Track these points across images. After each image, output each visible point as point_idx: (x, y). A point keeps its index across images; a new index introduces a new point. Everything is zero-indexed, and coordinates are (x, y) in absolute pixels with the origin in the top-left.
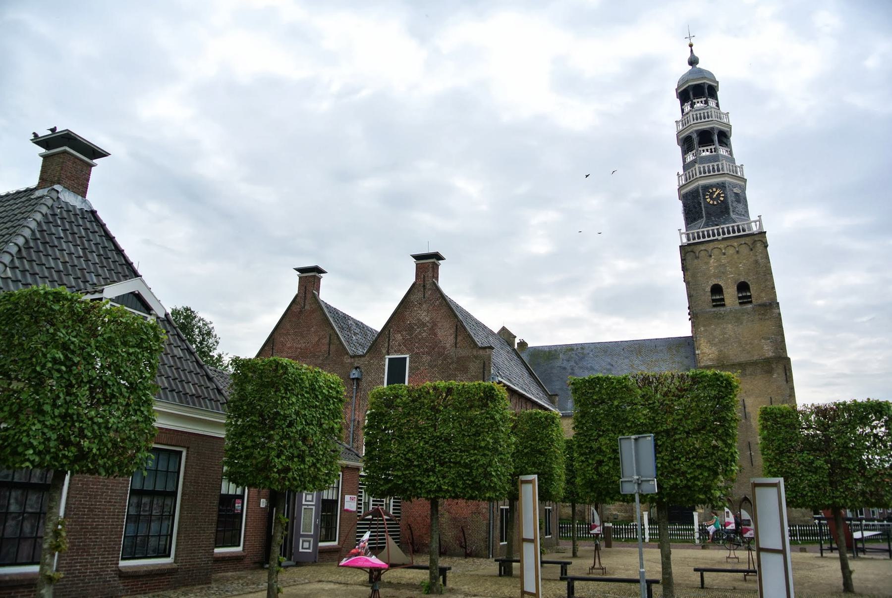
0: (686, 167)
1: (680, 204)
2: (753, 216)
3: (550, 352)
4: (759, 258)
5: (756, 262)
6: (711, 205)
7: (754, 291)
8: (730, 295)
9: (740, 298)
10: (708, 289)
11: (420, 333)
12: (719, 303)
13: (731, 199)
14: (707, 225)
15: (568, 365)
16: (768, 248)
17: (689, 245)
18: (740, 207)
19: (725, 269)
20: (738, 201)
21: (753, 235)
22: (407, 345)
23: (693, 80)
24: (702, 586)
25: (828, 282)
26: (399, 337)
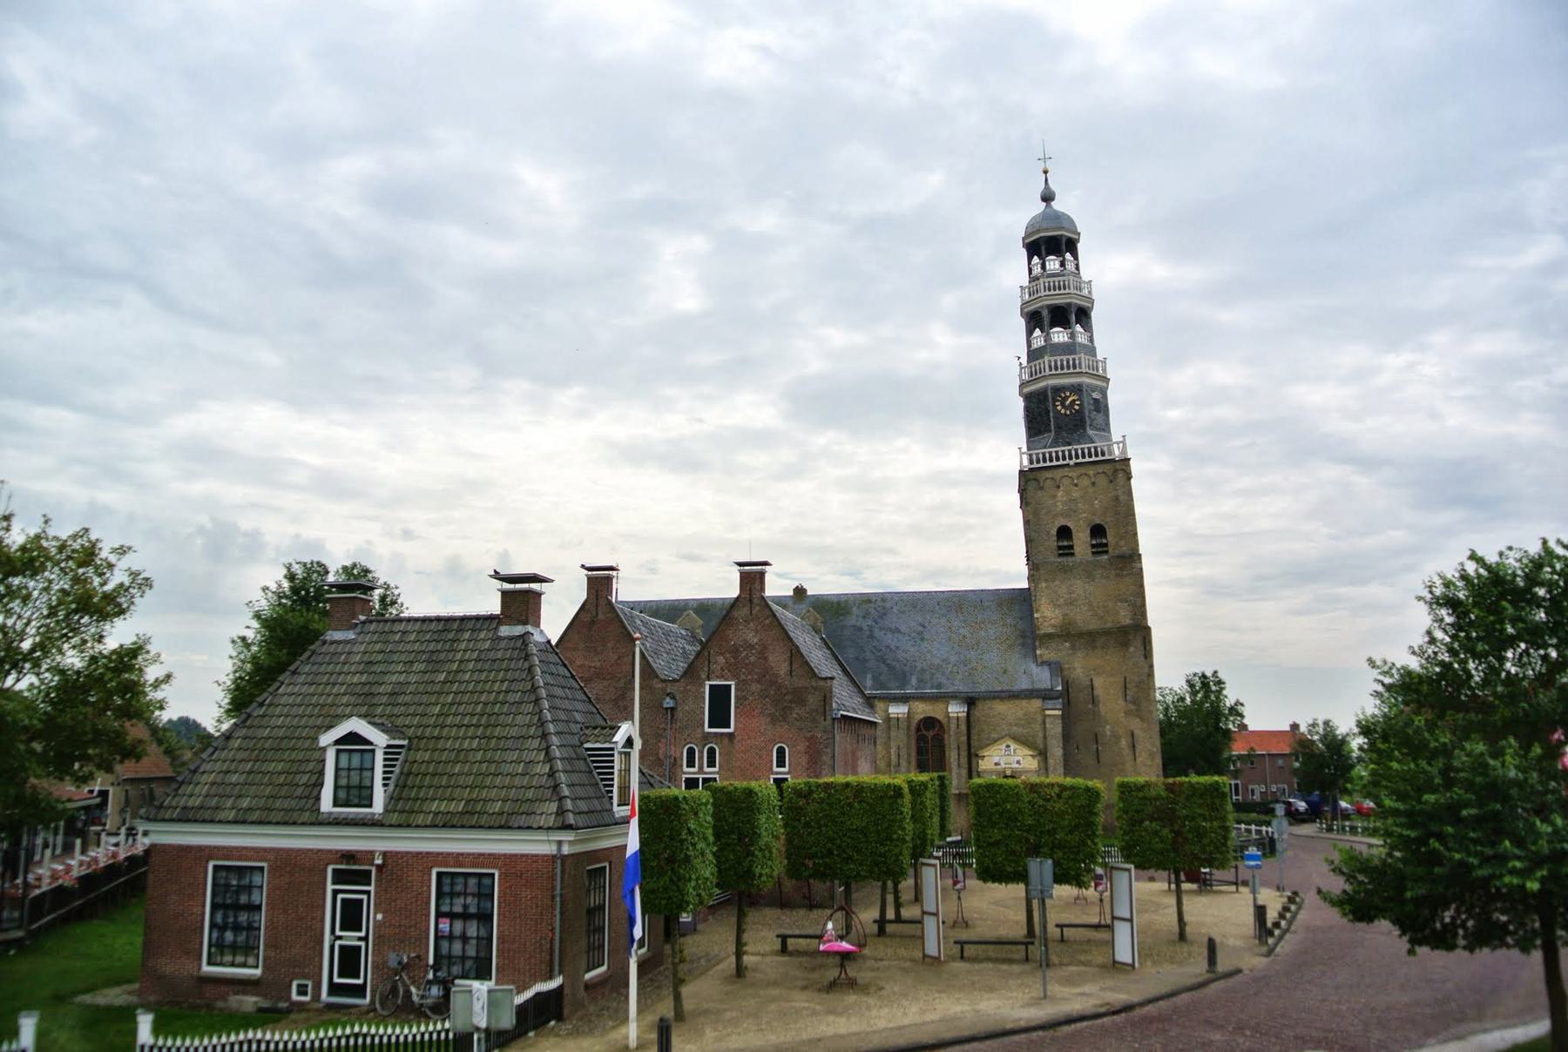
0: (1033, 355)
1: (1020, 404)
2: (1116, 435)
3: (839, 603)
4: (1120, 492)
5: (1116, 498)
6: (1062, 414)
7: (1111, 538)
8: (1082, 540)
9: (1093, 546)
10: (1054, 532)
11: (747, 657)
12: (1067, 551)
13: (1088, 407)
14: (1055, 443)
15: (865, 624)
16: (1133, 481)
17: (1031, 470)
18: (1100, 418)
19: (1075, 504)
20: (1098, 410)
21: (1113, 461)
22: (733, 670)
23: (1047, 230)
24: (1062, 940)
25: (1184, 378)
26: (721, 659)
